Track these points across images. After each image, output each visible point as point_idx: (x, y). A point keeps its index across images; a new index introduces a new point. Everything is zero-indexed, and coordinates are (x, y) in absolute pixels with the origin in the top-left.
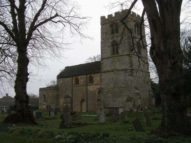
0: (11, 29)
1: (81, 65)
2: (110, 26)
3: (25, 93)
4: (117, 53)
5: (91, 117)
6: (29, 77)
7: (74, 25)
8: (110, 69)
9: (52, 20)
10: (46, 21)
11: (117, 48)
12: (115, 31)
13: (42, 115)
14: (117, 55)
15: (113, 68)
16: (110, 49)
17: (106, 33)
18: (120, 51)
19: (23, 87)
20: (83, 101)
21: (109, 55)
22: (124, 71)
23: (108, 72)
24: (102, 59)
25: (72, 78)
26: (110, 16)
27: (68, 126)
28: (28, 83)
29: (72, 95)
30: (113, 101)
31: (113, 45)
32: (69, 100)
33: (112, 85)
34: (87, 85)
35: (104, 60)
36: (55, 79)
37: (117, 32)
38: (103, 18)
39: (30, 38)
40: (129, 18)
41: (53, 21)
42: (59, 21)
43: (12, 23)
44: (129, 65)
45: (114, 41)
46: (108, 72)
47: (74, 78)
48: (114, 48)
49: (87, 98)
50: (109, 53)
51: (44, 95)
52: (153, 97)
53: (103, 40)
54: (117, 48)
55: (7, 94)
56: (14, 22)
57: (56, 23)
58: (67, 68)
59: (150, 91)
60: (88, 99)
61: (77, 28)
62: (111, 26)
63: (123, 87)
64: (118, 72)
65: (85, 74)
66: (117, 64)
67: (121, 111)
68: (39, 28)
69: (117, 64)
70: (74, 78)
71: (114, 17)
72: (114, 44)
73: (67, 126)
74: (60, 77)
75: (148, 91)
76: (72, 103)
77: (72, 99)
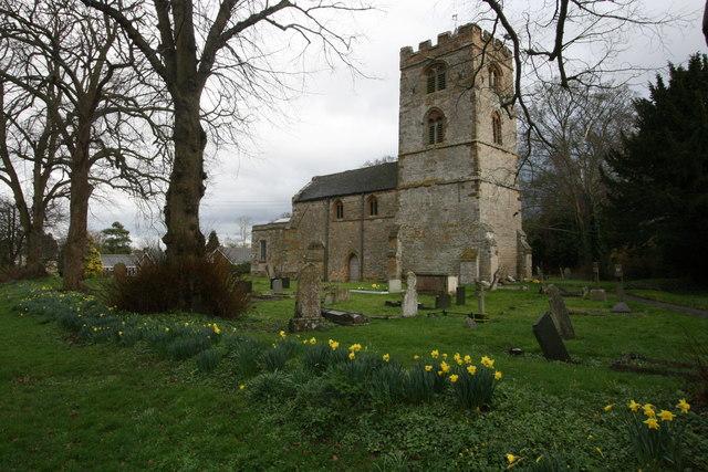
0: (154, 46)
1: (348, 173)
3: (195, 227)
4: (441, 140)
5: (371, 295)
6: (204, 183)
7: (336, 42)
8: (420, 180)
9: (269, 17)
10: (253, 20)
11: (440, 126)
12: (437, 83)
13: (255, 288)
14: (440, 145)
15: (429, 177)
16: (424, 129)
18: (448, 134)
20: (352, 256)
21: (420, 146)
23: (416, 187)
24: (401, 156)
26: (425, 45)
27: (314, 326)
28: (203, 201)
31: (431, 121)
33: (425, 219)
34: (362, 220)
35: (407, 158)
36: (289, 208)
37: (442, 86)
38: (406, 52)
39: (206, 72)
41: (273, 23)
42: (292, 26)
43: (158, 26)
44: (471, 170)
45: (433, 111)
46: (416, 187)
48: (432, 128)
49: (362, 250)
50: (418, 140)
51: (264, 242)
54: (440, 126)
56: (163, 25)
57: (284, 29)
58: (316, 179)
59: (519, 236)
60: (365, 253)
61: (343, 49)
62: (428, 71)
63: (452, 225)
64: (442, 187)
65: (360, 194)
66: (440, 166)
67: (453, 284)
68: (233, 42)
69: (440, 166)
70: (331, 204)
71: (437, 47)
72: (434, 116)
73: (310, 325)
74: (300, 200)
76: (326, 261)
77: (326, 252)
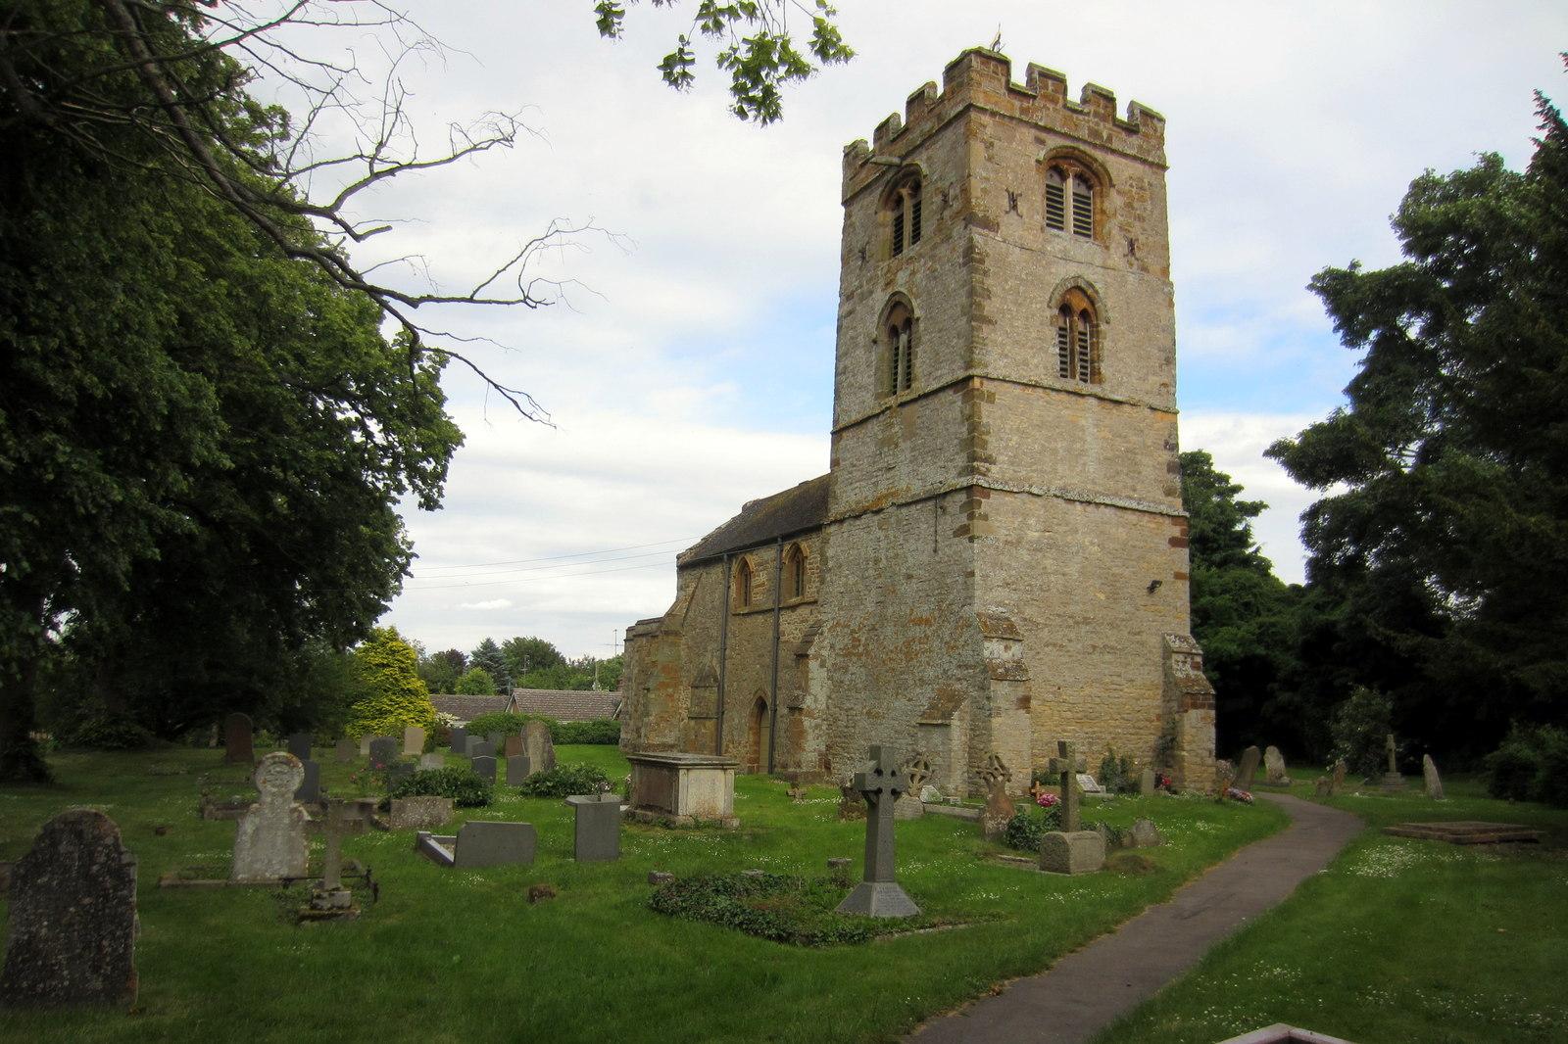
2: (886, 202)
17: (863, 252)
19: (1526, 496)
22: (930, 504)
25: (781, 546)
29: (723, 668)
30: (869, 713)
32: (711, 695)
40: (983, 110)
47: (787, 547)
52: (1193, 701)
53: (847, 307)
55: (659, 67)
59: (1168, 652)
70: (787, 547)
75: (1158, 659)
